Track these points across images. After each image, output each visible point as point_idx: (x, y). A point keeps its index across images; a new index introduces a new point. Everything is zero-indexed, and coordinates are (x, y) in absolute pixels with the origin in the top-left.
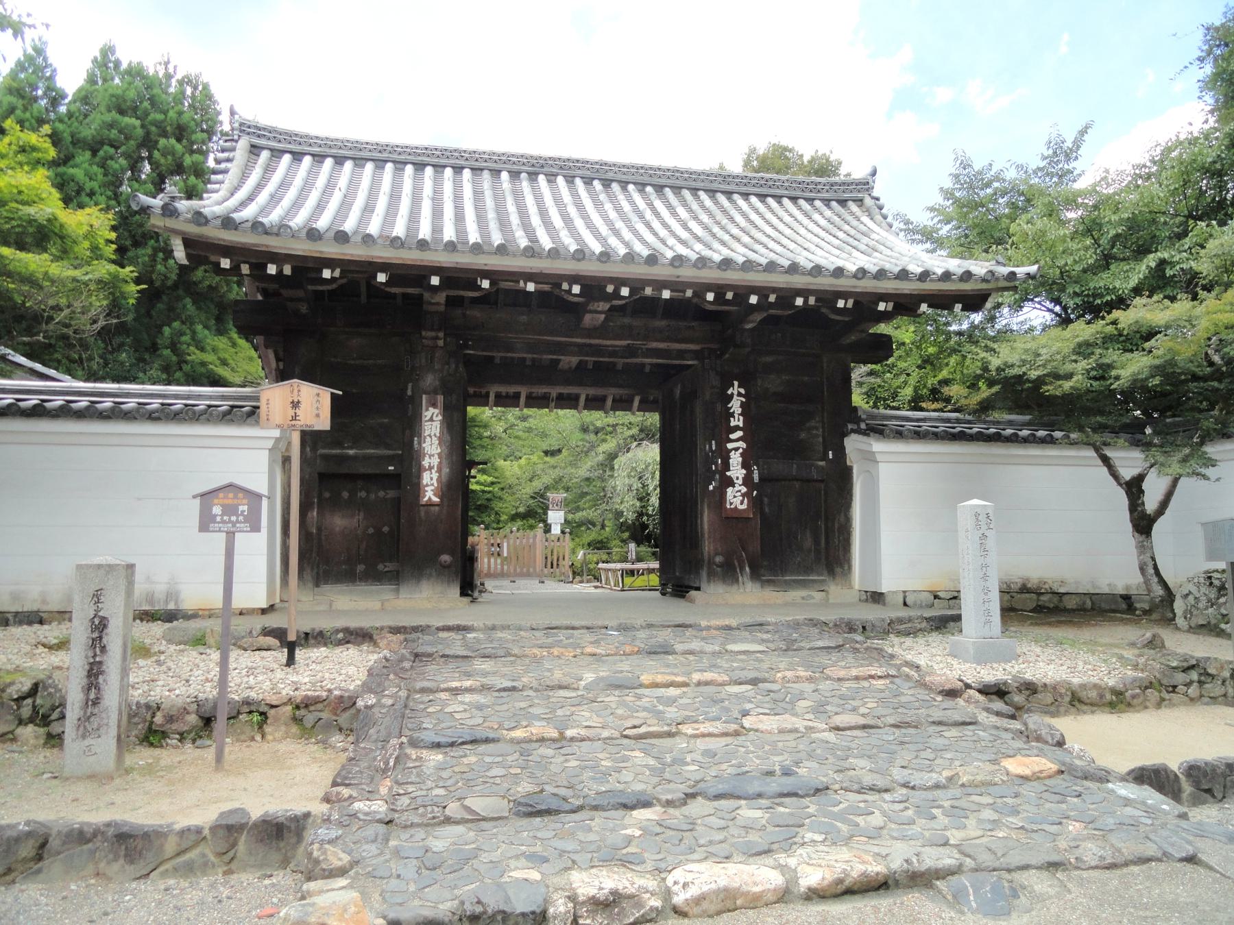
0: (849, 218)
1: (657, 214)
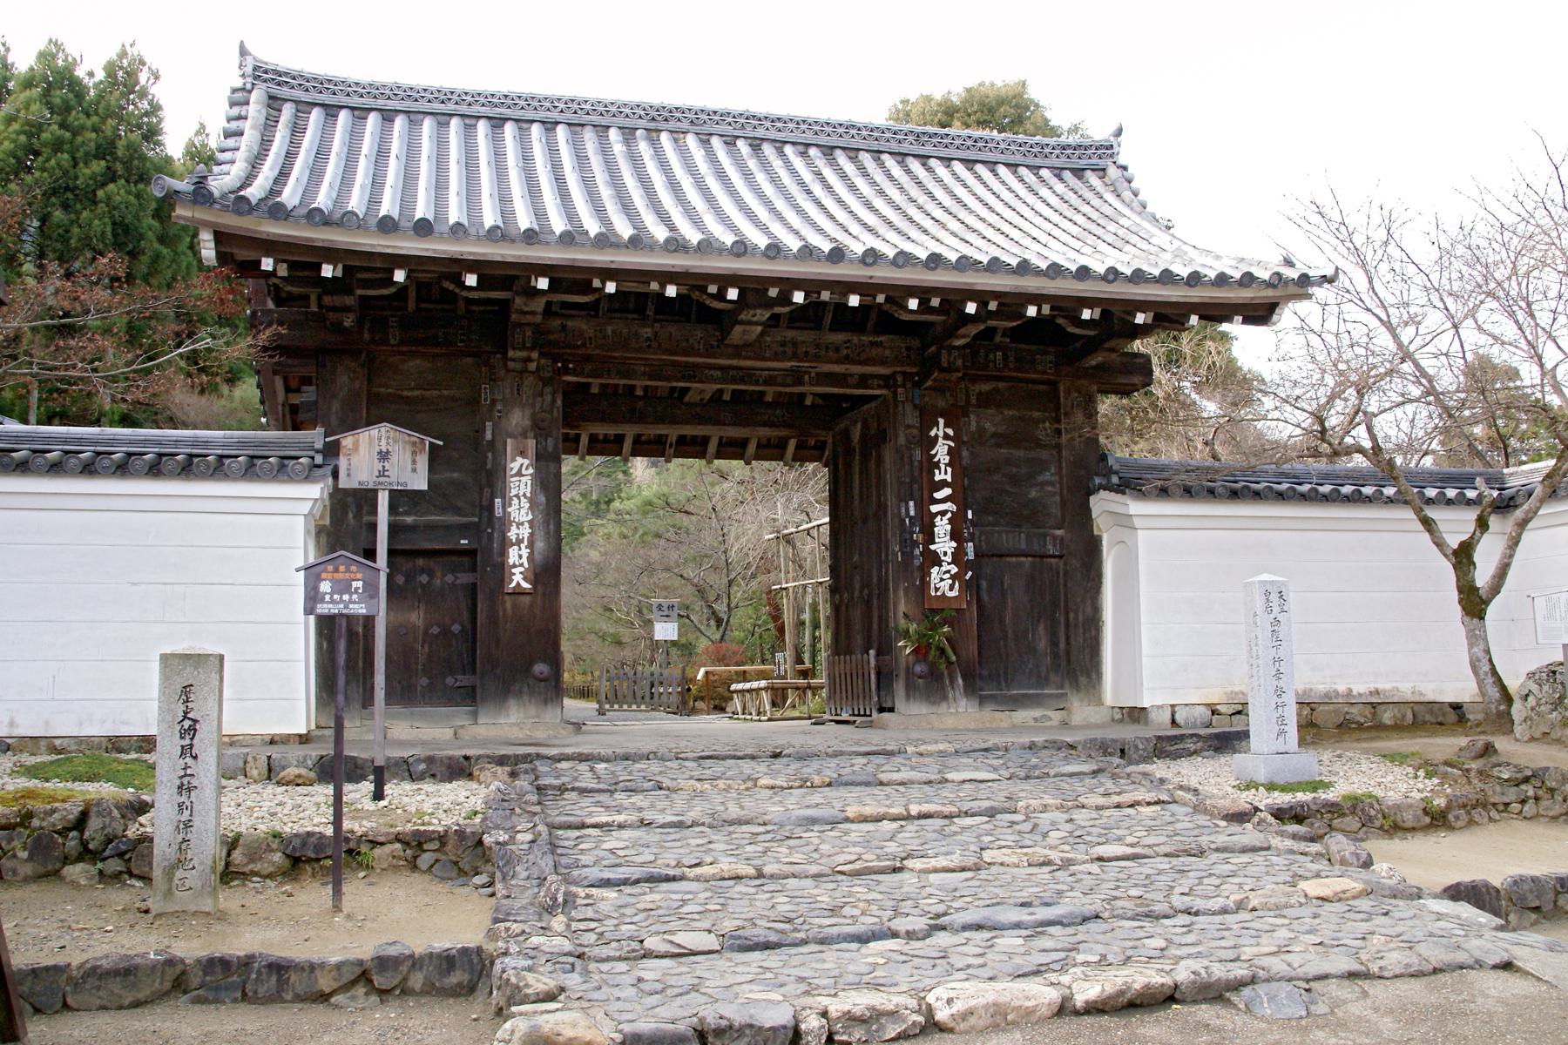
0: (1089, 195)
1: (828, 187)
